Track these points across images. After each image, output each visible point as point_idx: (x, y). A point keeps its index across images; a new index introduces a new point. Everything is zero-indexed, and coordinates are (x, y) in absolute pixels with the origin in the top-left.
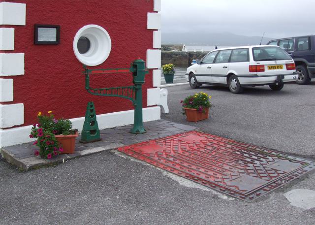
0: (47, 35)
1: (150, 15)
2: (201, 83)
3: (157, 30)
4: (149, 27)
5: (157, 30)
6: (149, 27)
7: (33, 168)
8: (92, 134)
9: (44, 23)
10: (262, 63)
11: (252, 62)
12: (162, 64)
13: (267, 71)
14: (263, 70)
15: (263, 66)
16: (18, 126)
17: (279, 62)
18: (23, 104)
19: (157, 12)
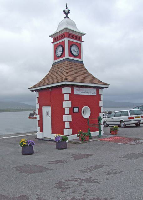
0: (76, 110)
2: (108, 125)
7: (81, 143)
8: (90, 137)
9: (75, 106)
10: (133, 116)
11: (129, 116)
13: (135, 119)
14: (133, 119)
15: (133, 117)
16: (70, 135)
17: (139, 115)
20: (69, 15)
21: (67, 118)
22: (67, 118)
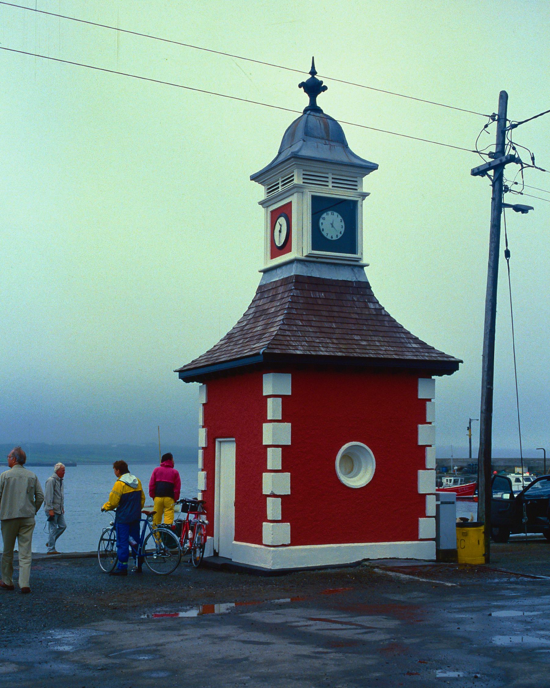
1: (422, 428)
3: (430, 446)
4: (421, 443)
5: (430, 446)
6: (421, 443)
12: (454, 459)
18: (289, 524)
19: (430, 423)
20: (321, 100)
21: (276, 483)
22: (276, 483)
